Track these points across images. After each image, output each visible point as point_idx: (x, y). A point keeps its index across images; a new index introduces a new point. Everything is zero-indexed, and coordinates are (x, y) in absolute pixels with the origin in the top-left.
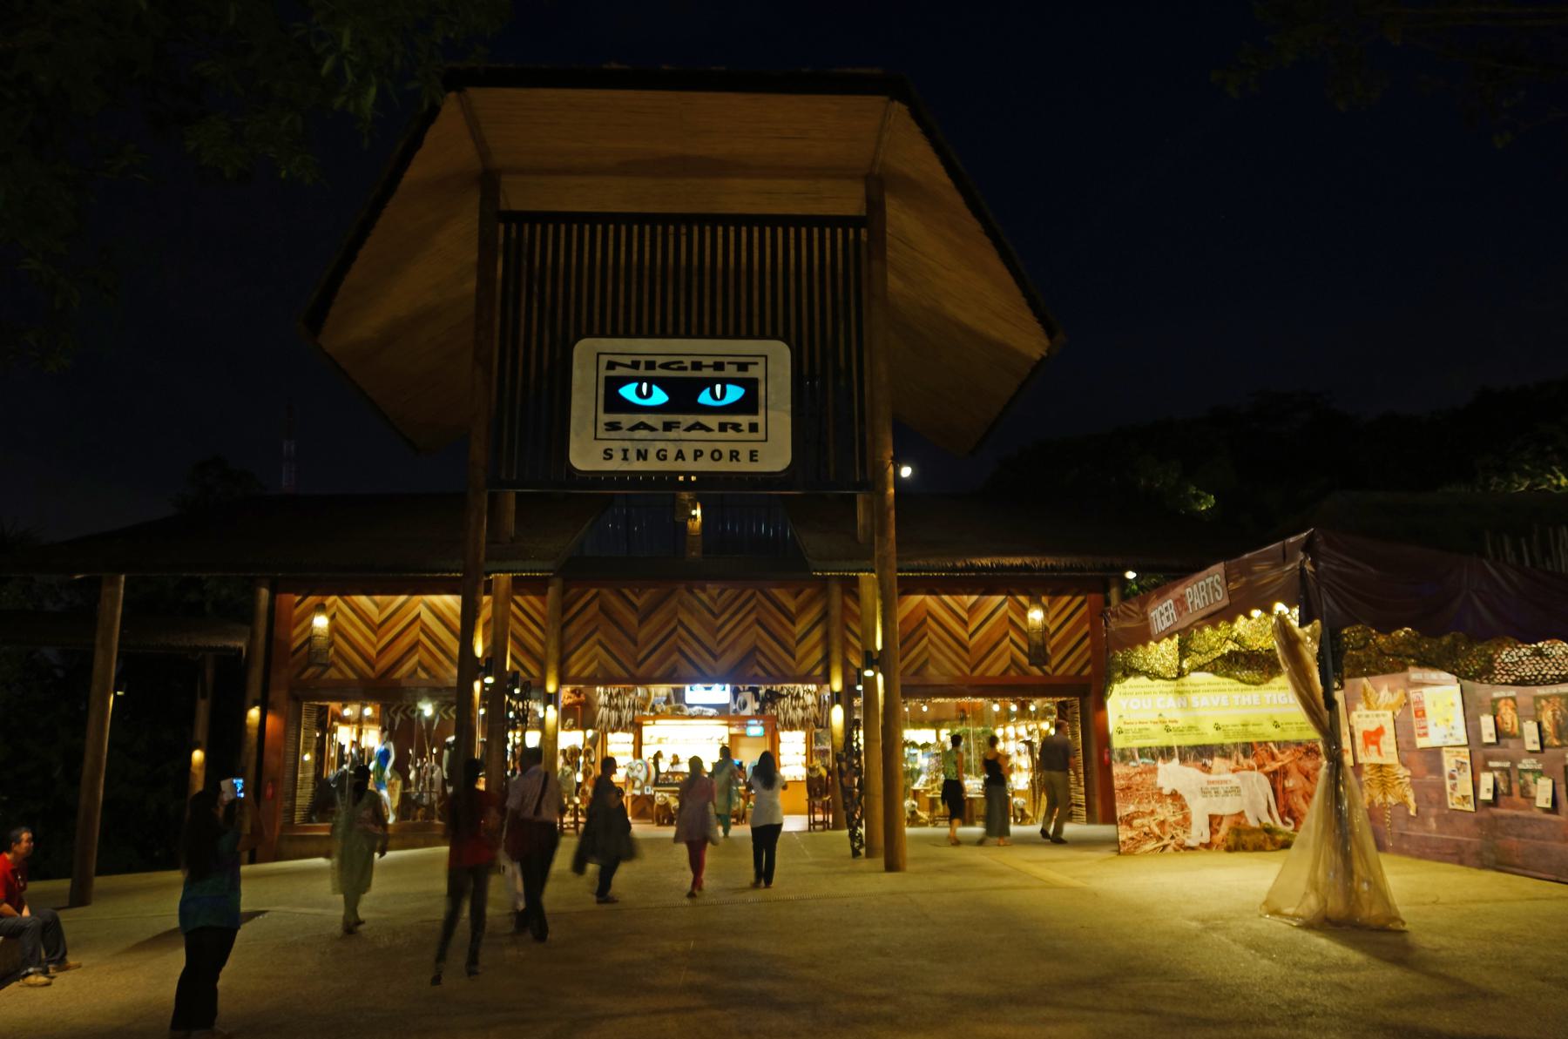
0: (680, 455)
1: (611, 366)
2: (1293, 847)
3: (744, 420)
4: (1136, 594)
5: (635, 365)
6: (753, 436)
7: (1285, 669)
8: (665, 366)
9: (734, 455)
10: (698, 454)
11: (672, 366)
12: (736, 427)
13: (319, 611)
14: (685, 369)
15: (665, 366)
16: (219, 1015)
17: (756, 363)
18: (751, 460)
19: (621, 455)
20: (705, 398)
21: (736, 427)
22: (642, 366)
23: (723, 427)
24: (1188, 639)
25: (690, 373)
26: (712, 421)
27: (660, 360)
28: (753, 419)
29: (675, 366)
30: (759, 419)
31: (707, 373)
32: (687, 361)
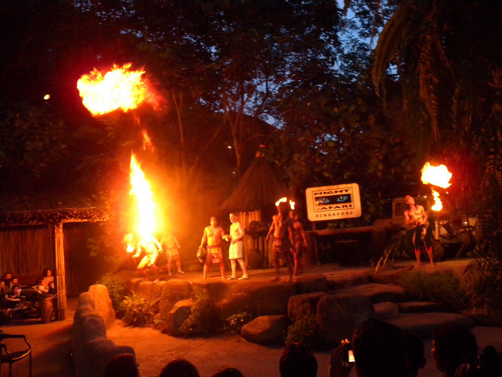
0: (334, 215)
1: (316, 194)
2: (413, 265)
3: (348, 204)
4: (231, 83)
5: (321, 193)
6: (351, 208)
7: (280, 214)
8: (328, 193)
9: (347, 213)
10: (338, 214)
11: (330, 193)
12: (346, 206)
13: (181, 286)
14: (332, 193)
15: (328, 193)
16: (198, 367)
17: (349, 190)
18: (351, 214)
19: (322, 216)
20: (338, 200)
21: (346, 206)
22: (323, 193)
23: (343, 206)
24: (74, 218)
25: (334, 194)
26: (340, 205)
27: (327, 191)
28: (350, 204)
29: (330, 193)
30: (352, 204)
31: (339, 193)
32: (334, 191)
